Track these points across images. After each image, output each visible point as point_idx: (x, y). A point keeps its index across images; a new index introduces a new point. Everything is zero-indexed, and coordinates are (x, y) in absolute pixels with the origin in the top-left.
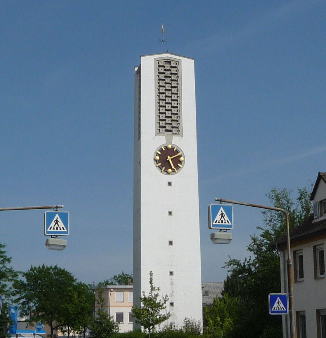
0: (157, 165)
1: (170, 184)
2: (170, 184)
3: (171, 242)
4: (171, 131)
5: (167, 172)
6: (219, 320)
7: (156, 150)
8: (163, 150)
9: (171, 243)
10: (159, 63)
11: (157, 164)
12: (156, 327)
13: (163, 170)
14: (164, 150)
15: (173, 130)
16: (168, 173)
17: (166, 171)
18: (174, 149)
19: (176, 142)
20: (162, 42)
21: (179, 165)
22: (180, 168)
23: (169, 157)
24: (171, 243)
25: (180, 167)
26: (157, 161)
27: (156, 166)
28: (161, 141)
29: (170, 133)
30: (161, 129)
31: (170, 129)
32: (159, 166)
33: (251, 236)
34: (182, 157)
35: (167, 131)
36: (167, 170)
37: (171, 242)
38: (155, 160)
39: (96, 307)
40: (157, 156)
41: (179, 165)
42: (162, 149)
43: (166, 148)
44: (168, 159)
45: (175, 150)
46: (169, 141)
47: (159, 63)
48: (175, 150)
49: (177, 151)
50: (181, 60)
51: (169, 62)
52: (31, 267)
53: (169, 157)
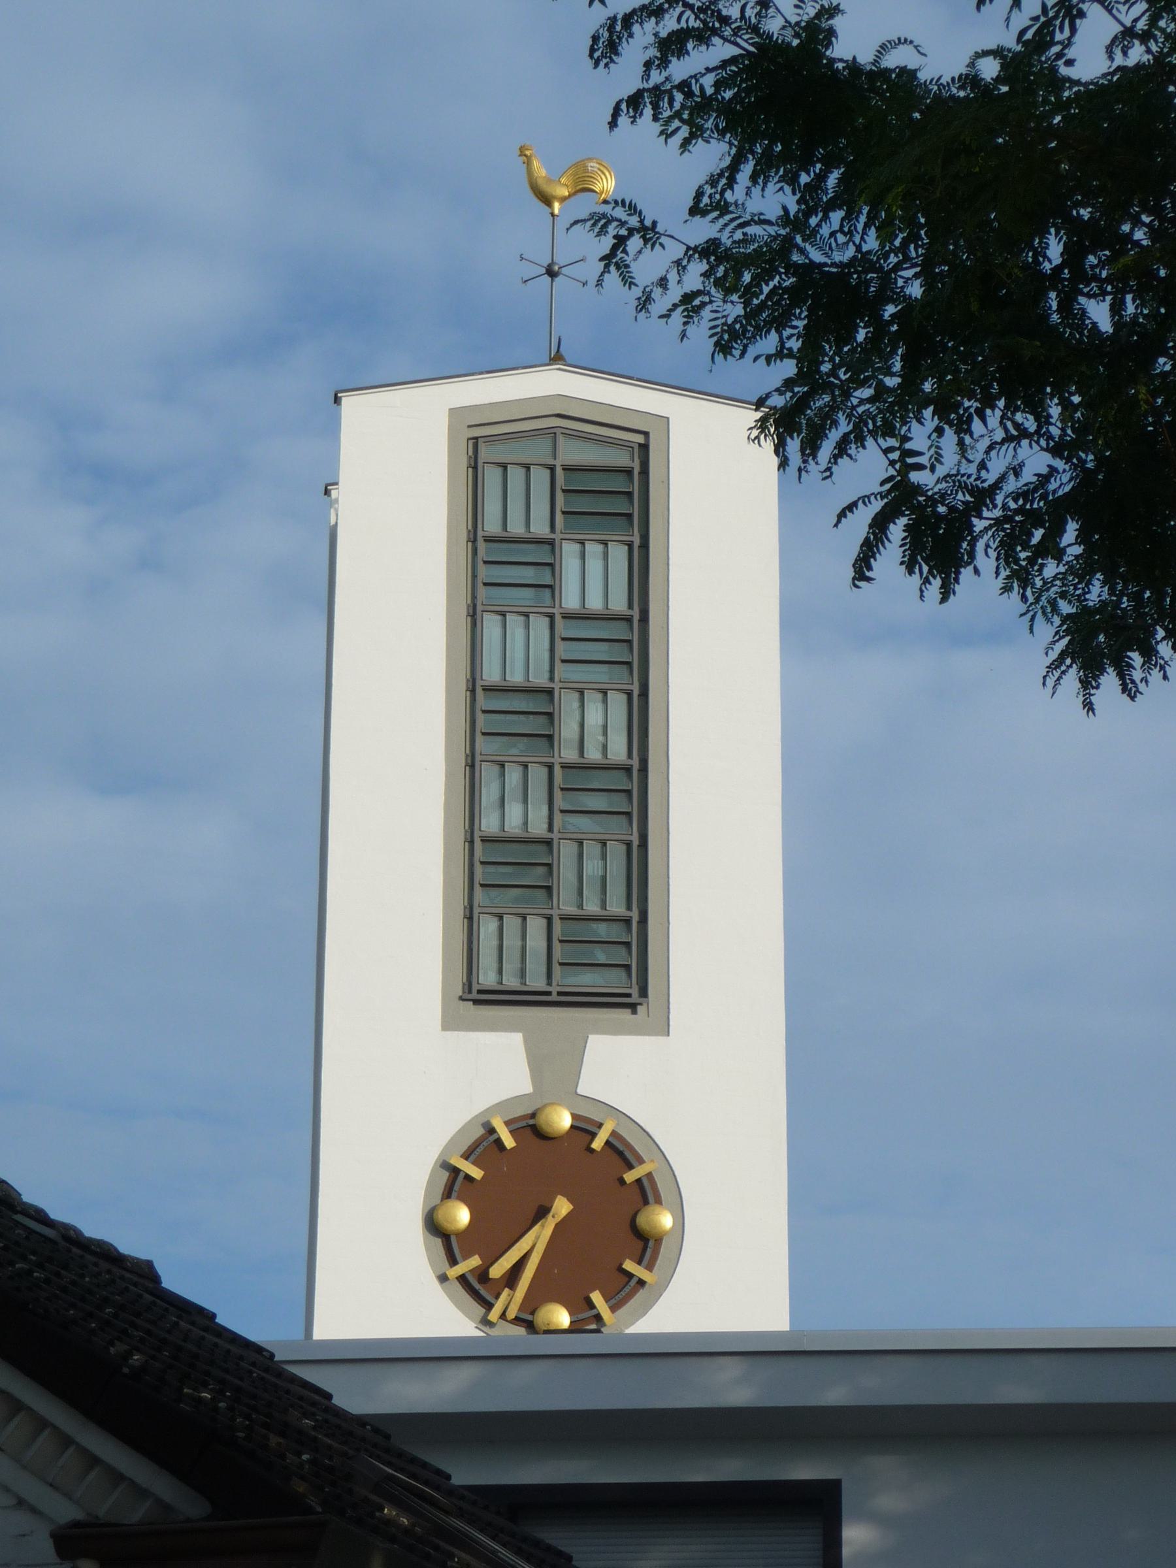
6: (1055, 307)
7: (448, 1148)
8: (499, 1142)
13: (494, 1316)
14: (509, 1142)
17: (529, 1318)
18: (593, 1135)
19: (619, 1073)
20: (547, 279)
22: (641, 1294)
25: (641, 1283)
26: (453, 1239)
27: (443, 1278)
28: (492, 1070)
32: (462, 1279)
33: (1165, 677)
34: (658, 1201)
36: (533, 1313)
38: (434, 1226)
39: (603, 905)
40: (448, 1194)
42: (494, 1137)
43: (530, 1128)
45: (597, 1144)
46: (555, 1066)
48: (597, 1144)
49: (621, 1154)
50: (646, 434)
52: (685, 278)
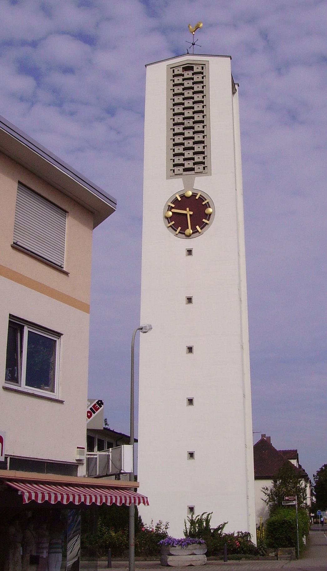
0: (177, 232)
1: (190, 252)
2: (190, 252)
3: (193, 508)
4: (193, 169)
5: (184, 234)
9: (191, 455)
10: (174, 70)
11: (176, 231)
12: (185, 515)
15: (196, 167)
16: (188, 236)
19: (201, 185)
21: (204, 203)
23: (191, 213)
24: (191, 455)
28: (177, 187)
29: (193, 172)
30: (176, 169)
31: (191, 166)
34: (210, 207)
35: (185, 170)
37: (193, 508)
41: (204, 203)
44: (188, 209)
46: (189, 185)
47: (174, 70)
51: (188, 68)
53: (191, 213)
